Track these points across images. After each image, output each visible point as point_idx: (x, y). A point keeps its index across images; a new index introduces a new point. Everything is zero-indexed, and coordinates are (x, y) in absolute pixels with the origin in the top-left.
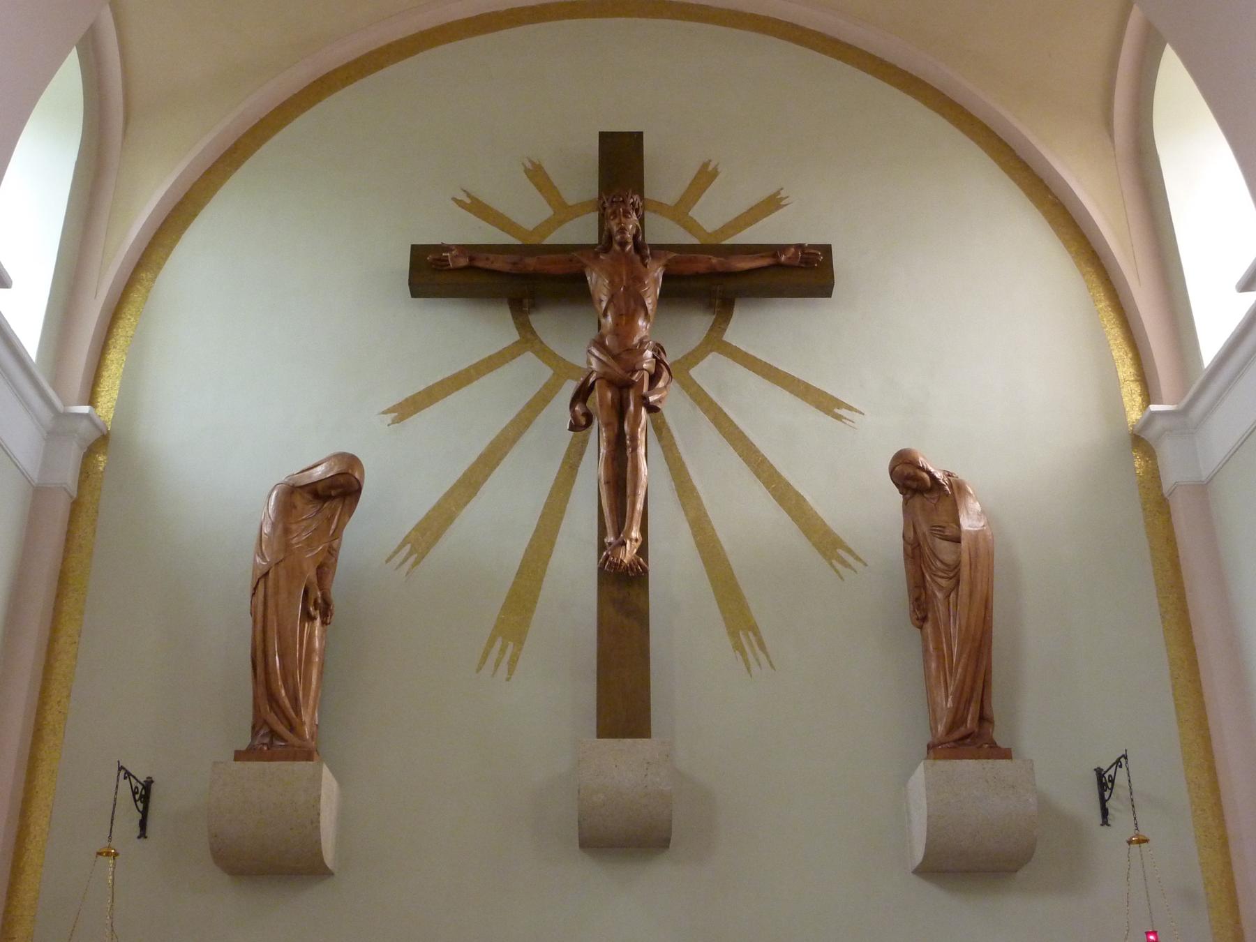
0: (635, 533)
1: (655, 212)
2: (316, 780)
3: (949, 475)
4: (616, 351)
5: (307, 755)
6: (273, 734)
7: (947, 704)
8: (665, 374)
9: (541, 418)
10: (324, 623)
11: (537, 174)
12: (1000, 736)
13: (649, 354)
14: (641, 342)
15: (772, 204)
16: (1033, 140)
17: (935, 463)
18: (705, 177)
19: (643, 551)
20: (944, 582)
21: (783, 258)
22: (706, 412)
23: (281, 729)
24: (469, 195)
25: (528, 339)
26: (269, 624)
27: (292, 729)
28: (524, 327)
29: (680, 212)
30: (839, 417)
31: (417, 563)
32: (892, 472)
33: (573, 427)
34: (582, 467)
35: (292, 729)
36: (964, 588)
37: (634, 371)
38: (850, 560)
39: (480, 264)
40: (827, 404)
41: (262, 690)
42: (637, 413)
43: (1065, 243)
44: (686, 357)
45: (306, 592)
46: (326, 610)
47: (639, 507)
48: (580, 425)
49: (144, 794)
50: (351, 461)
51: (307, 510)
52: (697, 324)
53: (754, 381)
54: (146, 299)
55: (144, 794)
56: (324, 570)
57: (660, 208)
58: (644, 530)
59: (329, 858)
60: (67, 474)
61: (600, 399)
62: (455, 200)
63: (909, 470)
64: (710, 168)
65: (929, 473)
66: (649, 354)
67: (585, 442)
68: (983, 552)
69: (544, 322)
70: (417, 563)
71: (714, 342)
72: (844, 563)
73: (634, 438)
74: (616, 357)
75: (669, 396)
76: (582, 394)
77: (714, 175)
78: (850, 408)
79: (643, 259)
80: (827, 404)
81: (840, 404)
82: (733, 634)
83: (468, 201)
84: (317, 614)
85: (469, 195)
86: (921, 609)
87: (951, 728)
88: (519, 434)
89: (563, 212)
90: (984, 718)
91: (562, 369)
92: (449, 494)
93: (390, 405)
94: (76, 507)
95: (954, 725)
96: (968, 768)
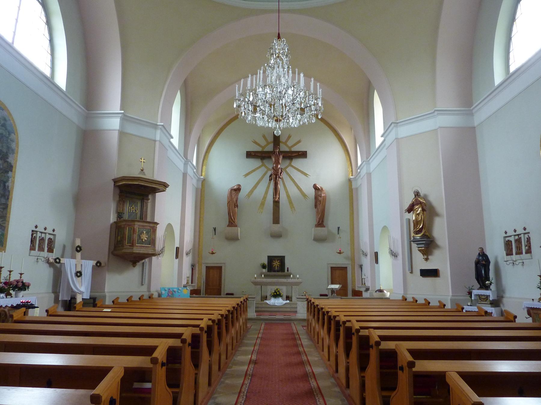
0: (278, 196)
1: (282, 143)
2: (238, 230)
3: (321, 187)
4: (276, 170)
5: (236, 226)
6: (232, 223)
7: (318, 220)
8: (282, 172)
9: (264, 179)
10: (237, 208)
11: (264, 137)
12: (324, 224)
13: (280, 170)
14: (279, 168)
15: (299, 142)
16: (340, 132)
17: (318, 186)
18: (289, 137)
19: (279, 198)
20: (319, 203)
21: (300, 154)
22: (288, 176)
23: (233, 223)
24: (254, 140)
25: (263, 165)
26: (274, 321)
27: (234, 222)
28: (262, 162)
29: (285, 143)
30: (307, 177)
31: (249, 198)
32: (313, 187)
33: (270, 180)
34: (270, 187)
35: (234, 222)
36: (321, 204)
37: (278, 173)
38: (308, 198)
39: (256, 155)
40: (306, 174)
41: (230, 217)
42: (278, 179)
43: (343, 148)
44: (286, 167)
45: (235, 204)
46: (237, 206)
47: (278, 192)
48: (270, 180)
49: (215, 229)
50: (239, 185)
51: (233, 192)
52: (287, 162)
53: (295, 171)
54: (208, 158)
55: (215, 229)
56: (236, 201)
57: (283, 143)
58: (279, 195)
59: (239, 238)
60: (200, 186)
61: (274, 176)
62: (252, 141)
63: (315, 187)
64: (290, 135)
65: (318, 187)
66: (280, 170)
67: (271, 182)
68: (325, 199)
69: (266, 162)
70: (249, 198)
71: (290, 165)
72: (307, 198)
73: (278, 183)
74: (276, 171)
75: (284, 175)
76: (271, 176)
77: (291, 136)
78: (309, 175)
79: (280, 155)
80: (306, 174)
81: (308, 175)
82: (306, 176)
83: (254, 141)
84: (236, 207)
85: (254, 140)
86: (316, 206)
87: (318, 223)
88: (262, 179)
89: (268, 143)
90: (323, 221)
91: (268, 169)
92: (252, 188)
93: (244, 174)
94: (201, 190)
95: (319, 222)
96: (319, 228)
